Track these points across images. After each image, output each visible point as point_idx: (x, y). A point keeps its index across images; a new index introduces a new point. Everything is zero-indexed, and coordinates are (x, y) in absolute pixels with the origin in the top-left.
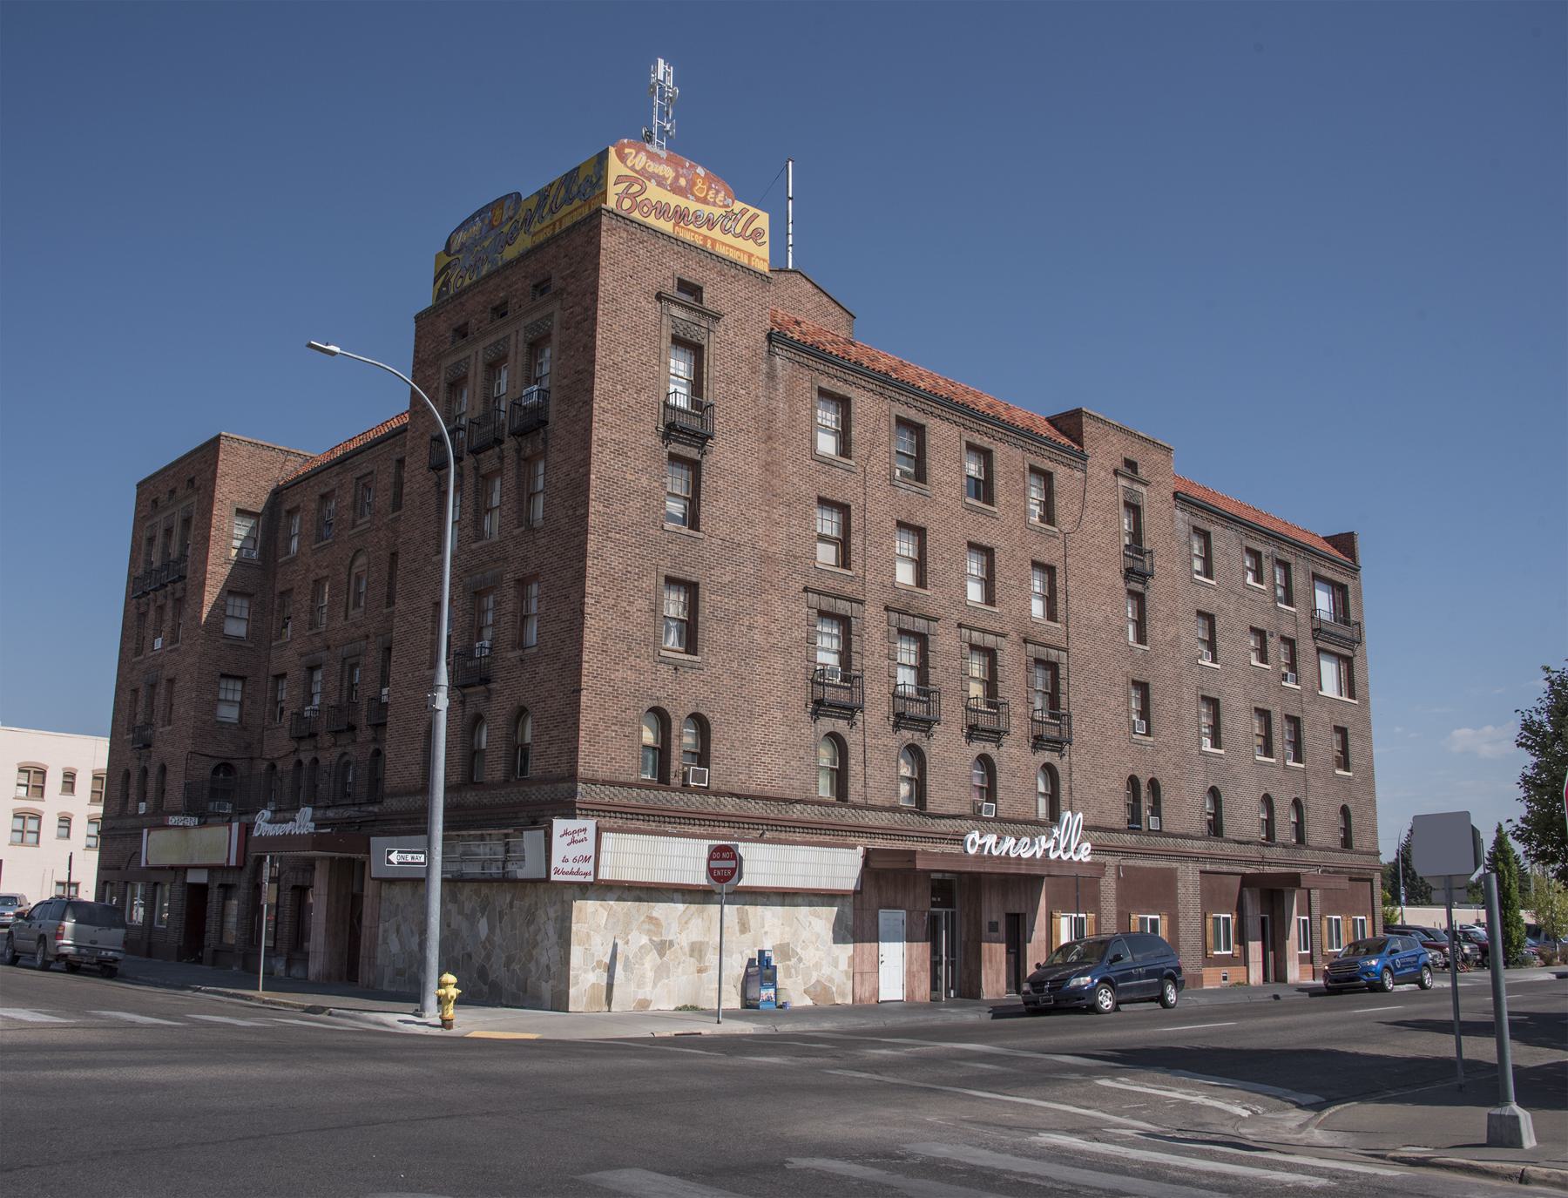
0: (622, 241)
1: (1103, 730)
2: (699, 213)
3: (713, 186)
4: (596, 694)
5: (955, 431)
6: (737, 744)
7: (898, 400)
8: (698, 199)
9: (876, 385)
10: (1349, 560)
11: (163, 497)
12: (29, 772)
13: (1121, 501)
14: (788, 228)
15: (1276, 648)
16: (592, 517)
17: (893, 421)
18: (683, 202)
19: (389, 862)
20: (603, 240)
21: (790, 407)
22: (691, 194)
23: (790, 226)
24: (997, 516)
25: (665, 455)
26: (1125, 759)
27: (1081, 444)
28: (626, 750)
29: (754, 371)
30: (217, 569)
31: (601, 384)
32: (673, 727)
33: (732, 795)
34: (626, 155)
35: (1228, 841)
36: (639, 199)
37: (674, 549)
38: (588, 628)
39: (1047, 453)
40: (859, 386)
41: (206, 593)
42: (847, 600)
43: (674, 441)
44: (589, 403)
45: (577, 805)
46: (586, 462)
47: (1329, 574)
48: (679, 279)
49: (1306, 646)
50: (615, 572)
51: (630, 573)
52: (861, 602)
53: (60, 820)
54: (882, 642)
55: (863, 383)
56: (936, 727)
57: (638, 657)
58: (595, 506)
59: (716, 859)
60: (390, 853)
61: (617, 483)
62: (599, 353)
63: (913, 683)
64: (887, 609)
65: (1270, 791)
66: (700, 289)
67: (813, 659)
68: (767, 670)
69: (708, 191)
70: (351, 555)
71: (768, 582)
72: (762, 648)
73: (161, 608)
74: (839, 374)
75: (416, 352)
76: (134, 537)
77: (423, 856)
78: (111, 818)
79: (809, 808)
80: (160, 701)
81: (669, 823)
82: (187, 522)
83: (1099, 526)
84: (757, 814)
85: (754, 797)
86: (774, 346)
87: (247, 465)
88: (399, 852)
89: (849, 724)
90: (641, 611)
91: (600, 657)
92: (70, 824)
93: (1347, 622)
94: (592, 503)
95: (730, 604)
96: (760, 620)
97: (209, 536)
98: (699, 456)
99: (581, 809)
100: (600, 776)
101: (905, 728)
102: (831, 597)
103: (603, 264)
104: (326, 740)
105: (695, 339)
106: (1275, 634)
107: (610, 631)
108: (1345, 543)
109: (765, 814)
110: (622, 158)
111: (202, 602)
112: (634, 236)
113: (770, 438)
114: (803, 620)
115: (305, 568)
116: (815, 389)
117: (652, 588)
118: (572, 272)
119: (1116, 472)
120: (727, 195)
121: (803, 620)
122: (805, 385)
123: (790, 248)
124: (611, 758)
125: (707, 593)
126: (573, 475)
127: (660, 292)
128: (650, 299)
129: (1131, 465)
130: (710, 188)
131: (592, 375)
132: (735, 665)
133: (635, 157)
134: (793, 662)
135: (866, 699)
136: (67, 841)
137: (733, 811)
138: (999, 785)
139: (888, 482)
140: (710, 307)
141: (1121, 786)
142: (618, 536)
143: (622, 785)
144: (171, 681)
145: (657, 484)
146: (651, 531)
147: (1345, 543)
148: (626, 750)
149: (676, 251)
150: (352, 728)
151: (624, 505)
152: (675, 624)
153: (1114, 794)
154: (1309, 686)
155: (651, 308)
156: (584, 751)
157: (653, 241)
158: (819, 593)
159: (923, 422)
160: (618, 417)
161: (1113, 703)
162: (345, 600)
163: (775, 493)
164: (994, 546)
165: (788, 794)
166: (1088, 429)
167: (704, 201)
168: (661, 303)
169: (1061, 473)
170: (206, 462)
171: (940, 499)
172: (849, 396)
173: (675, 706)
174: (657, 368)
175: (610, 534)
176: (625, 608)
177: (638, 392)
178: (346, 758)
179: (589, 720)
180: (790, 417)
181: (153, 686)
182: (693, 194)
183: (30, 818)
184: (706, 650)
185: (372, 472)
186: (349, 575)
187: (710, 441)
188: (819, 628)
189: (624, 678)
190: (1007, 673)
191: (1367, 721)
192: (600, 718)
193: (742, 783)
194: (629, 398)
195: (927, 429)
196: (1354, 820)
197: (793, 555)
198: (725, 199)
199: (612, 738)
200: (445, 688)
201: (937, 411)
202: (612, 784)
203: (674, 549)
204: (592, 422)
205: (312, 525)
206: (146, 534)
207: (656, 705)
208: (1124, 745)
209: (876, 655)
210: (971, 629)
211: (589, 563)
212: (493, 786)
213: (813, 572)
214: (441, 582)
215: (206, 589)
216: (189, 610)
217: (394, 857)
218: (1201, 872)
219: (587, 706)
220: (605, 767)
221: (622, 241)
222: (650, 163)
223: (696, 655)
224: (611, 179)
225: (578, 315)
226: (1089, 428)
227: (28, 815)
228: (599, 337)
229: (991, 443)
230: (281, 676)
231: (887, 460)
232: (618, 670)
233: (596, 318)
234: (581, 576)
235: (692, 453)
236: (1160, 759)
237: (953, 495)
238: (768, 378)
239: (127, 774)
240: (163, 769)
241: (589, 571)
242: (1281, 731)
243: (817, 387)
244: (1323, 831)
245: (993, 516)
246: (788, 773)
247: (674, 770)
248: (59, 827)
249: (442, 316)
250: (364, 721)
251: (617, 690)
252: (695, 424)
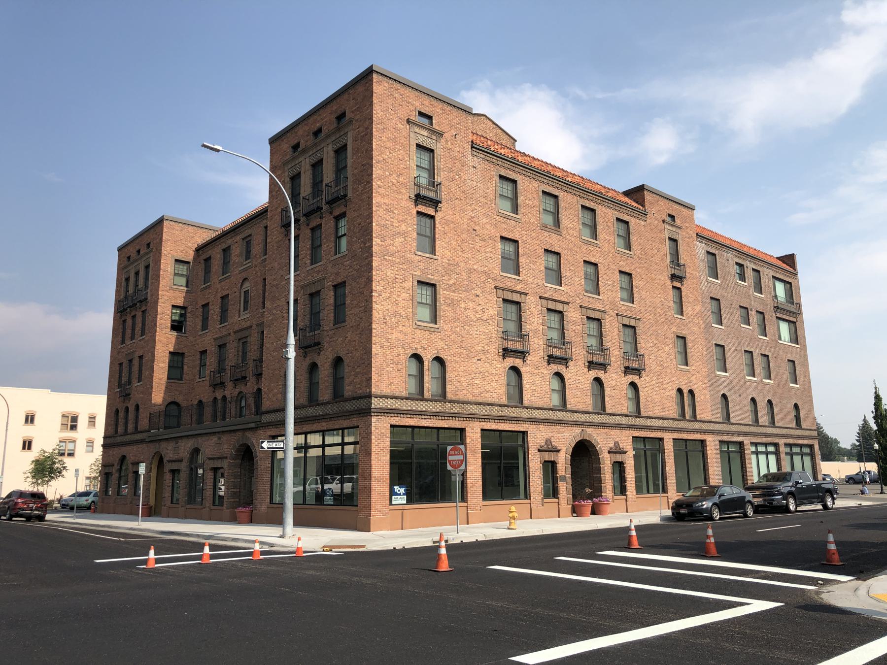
0: (385, 88)
1: (662, 363)
4: (381, 347)
7: (543, 182)
10: (792, 269)
11: (134, 256)
12: (68, 417)
13: (667, 237)
15: (754, 317)
17: (541, 194)
20: (374, 88)
24: (598, 246)
25: (415, 212)
26: (675, 379)
27: (643, 206)
30: (165, 293)
31: (377, 172)
39: (625, 211)
43: (420, 204)
44: (370, 182)
45: (372, 410)
46: (370, 216)
47: (781, 277)
48: (419, 111)
49: (770, 316)
50: (389, 279)
53: (87, 442)
55: (524, 172)
56: (571, 363)
58: (376, 241)
59: (452, 455)
61: (388, 228)
62: (375, 153)
63: (557, 339)
64: (541, 298)
70: (241, 281)
71: (475, 283)
73: (134, 317)
74: (510, 167)
76: (117, 278)
78: (110, 437)
80: (135, 368)
81: (425, 419)
82: (147, 267)
83: (655, 251)
90: (404, 300)
91: (382, 326)
92: (93, 444)
97: (160, 275)
104: (229, 385)
107: (387, 311)
108: (789, 260)
112: (392, 86)
115: (215, 290)
117: (410, 287)
118: (357, 108)
119: (664, 221)
122: (492, 174)
126: (363, 224)
129: (672, 217)
132: (458, 329)
135: (531, 348)
136: (91, 454)
141: (674, 393)
142: (390, 258)
143: (397, 398)
144: (141, 357)
145: (410, 229)
147: (789, 260)
149: (417, 95)
150: (244, 378)
155: (403, 127)
159: (557, 194)
161: (667, 349)
162: (238, 307)
169: (633, 221)
170: (156, 234)
171: (568, 237)
172: (516, 179)
173: (426, 353)
174: (408, 163)
175: (385, 257)
176: (395, 298)
177: (398, 176)
181: (131, 361)
184: (442, 321)
186: (240, 293)
187: (439, 204)
190: (607, 333)
191: (805, 357)
195: (559, 198)
196: (801, 411)
200: (293, 346)
201: (564, 188)
204: (372, 193)
205: (218, 267)
206: (124, 277)
207: (415, 352)
208: (674, 372)
211: (374, 273)
214: (289, 291)
215: (159, 304)
216: (150, 317)
218: (720, 441)
221: (385, 88)
225: (362, 132)
226: (648, 196)
227: (67, 441)
229: (595, 206)
230: (204, 352)
231: (538, 215)
232: (393, 333)
233: (372, 133)
234: (370, 280)
235: (430, 211)
236: (694, 379)
237: (575, 235)
239: (117, 411)
241: (374, 277)
242: (758, 361)
244: (784, 417)
245: (597, 246)
246: (489, 389)
248: (87, 446)
249: (285, 140)
250: (251, 373)
251: (392, 345)
252: (432, 195)
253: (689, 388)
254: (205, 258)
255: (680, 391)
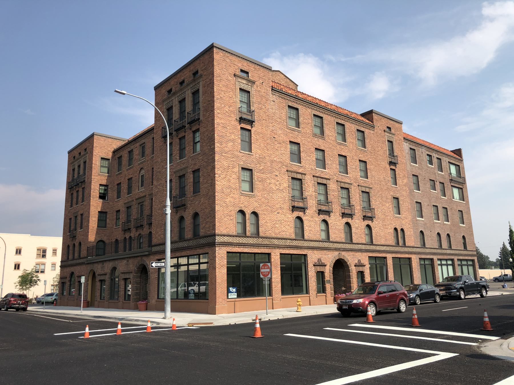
0: (221, 56)
1: (385, 213)
4: (221, 206)
5: (333, 119)
7: (314, 109)
11: (77, 156)
15: (438, 186)
16: (216, 149)
19: (152, 266)
24: (347, 146)
25: (239, 128)
26: (393, 222)
27: (372, 122)
31: (217, 105)
35: (427, 248)
39: (362, 125)
41: (92, 185)
45: (216, 243)
46: (213, 130)
49: (448, 185)
51: (230, 166)
53: (52, 265)
54: (312, 187)
55: (302, 104)
56: (332, 214)
58: (217, 145)
59: (263, 269)
60: (152, 263)
62: (215, 94)
64: (313, 176)
65: (439, 232)
73: (78, 191)
74: (294, 101)
75: (156, 100)
77: (164, 263)
78: (65, 261)
80: (79, 221)
81: (247, 248)
83: (380, 148)
87: (104, 143)
88: (155, 263)
90: (234, 179)
91: (221, 194)
92: (55, 266)
93: (461, 177)
94: (216, 144)
95: (263, 176)
101: (322, 214)
103: (215, 64)
106: (437, 181)
108: (458, 152)
109: (278, 244)
111: (91, 188)
119: (384, 131)
121: (287, 181)
127: (235, 74)
129: (389, 128)
131: (214, 102)
135: (308, 205)
136: (55, 271)
138: (353, 232)
139: (312, 136)
140: (252, 79)
141: (392, 231)
143: (230, 236)
144: (82, 215)
145: (237, 137)
146: (236, 153)
147: (458, 152)
153: (390, 234)
154: (449, 198)
155: (232, 79)
159: (322, 116)
164: (346, 156)
165: (285, 237)
166: (375, 117)
168: (235, 77)
169: (367, 131)
170: (90, 143)
171: (329, 141)
173: (247, 209)
174: (235, 99)
175: (223, 154)
177: (229, 107)
178: (140, 235)
181: (76, 217)
183: (42, 265)
185: (145, 143)
186: (139, 176)
189: (230, 201)
190: (353, 196)
191: (469, 208)
192: (222, 214)
193: (270, 234)
194: (227, 109)
196: (467, 240)
199: (226, 220)
200: (169, 207)
204: (214, 117)
208: (392, 218)
209: (311, 191)
210: (341, 182)
212: (189, 240)
215: (92, 184)
217: (154, 265)
220: (225, 230)
221: (221, 56)
226: (375, 116)
228: (215, 88)
229: (344, 122)
232: (228, 198)
233: (214, 82)
234: (214, 168)
235: (248, 127)
237: (333, 140)
239: (69, 246)
240: (80, 244)
241: (216, 166)
242: (441, 211)
244: (457, 244)
245: (346, 146)
248: (52, 267)
249: (163, 87)
251: (227, 205)
252: (249, 118)
253: (401, 228)
254: (118, 157)
255: (396, 229)
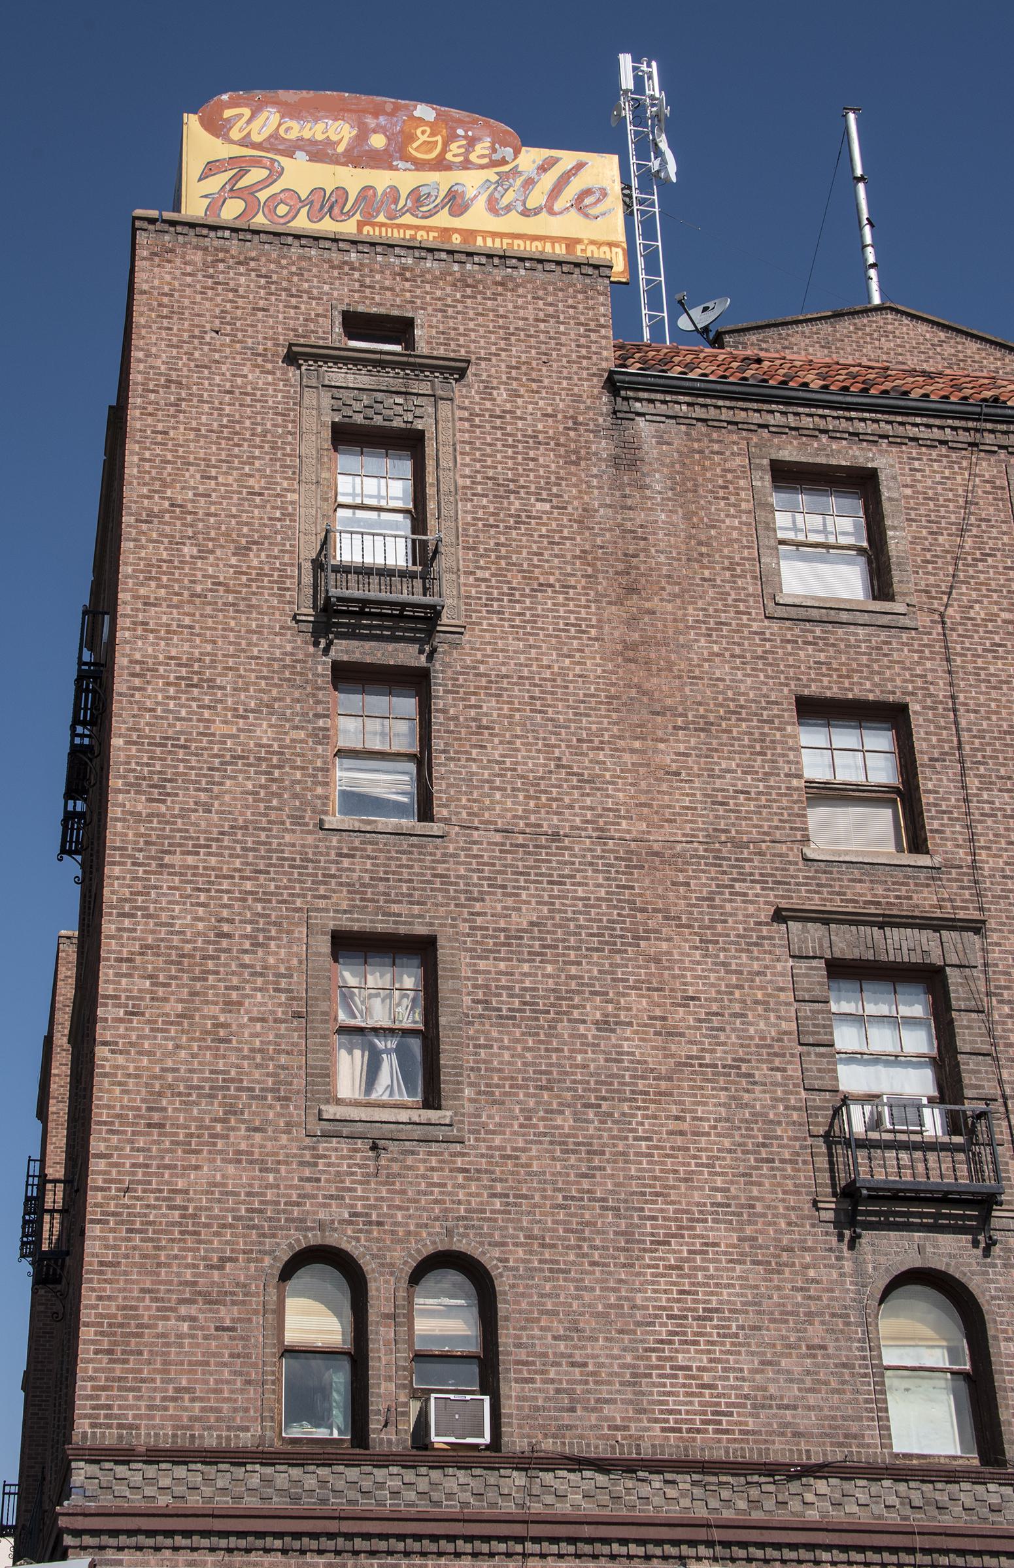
2: (424, 191)
3: (460, 132)
4: (130, 1231)
6: (588, 1324)
8: (420, 165)
9: (954, 429)
14: (862, 236)
18: (381, 179)
21: (687, 517)
22: (401, 159)
23: (867, 230)
28: (225, 1365)
29: (574, 458)
32: (372, 1292)
33: (578, 1463)
34: (228, 120)
36: (263, 196)
37: (359, 869)
38: (105, 1075)
40: (897, 441)
42: (921, 927)
45: (62, 1522)
51: (228, 936)
52: (977, 927)
57: (256, 1130)
66: (409, 323)
67: (827, 1083)
68: (672, 1125)
69: (446, 145)
71: (656, 910)
72: (652, 1070)
79: (860, 1489)
84: (673, 1511)
85: (656, 1466)
86: (626, 399)
89: (976, 1243)
90: (263, 1020)
91: (141, 1142)
96: (638, 1003)
98: (423, 658)
99: (77, 1533)
100: (142, 1439)
102: (864, 923)
105: (397, 423)
110: (216, 127)
113: (631, 590)
114: (782, 989)
116: (760, 467)
120: (499, 140)
121: (782, 989)
123: (873, 273)
124: (178, 1390)
125: (465, 958)
128: (269, 366)
130: (451, 137)
132: (566, 1121)
133: (249, 122)
134: (760, 1098)
137: (589, 1508)
142: (190, 860)
148: (225, 1365)
151: (206, 790)
152: (392, 1043)
156: (92, 1379)
157: (274, 255)
158: (825, 918)
160: (187, 608)
163: (657, 707)
165: (779, 1450)
167: (441, 164)
168: (299, 367)
173: (378, 1240)
175: (167, 859)
176: (215, 1017)
177: (242, 551)
179: (109, 1298)
180: (691, 537)
182: (406, 158)
184: (468, 1092)
188: (834, 1008)
189: (216, 1185)
192: (143, 1290)
197: (731, 840)
198: (494, 151)
202: (180, 1456)
203: (359, 869)
213: (800, 873)
219: (101, 1263)
221: (189, 269)
222: (289, 123)
223: (439, 1108)
224: (192, 166)
235: (405, 655)
238: (617, 466)
243: (766, 462)
247: (382, 1407)
